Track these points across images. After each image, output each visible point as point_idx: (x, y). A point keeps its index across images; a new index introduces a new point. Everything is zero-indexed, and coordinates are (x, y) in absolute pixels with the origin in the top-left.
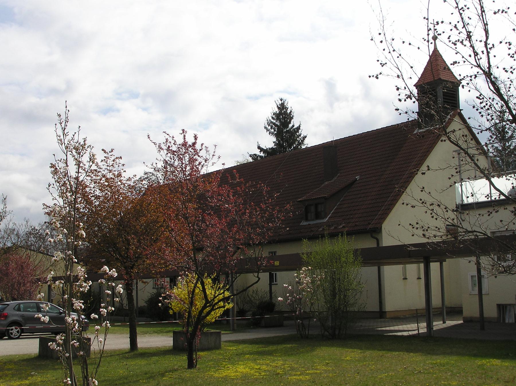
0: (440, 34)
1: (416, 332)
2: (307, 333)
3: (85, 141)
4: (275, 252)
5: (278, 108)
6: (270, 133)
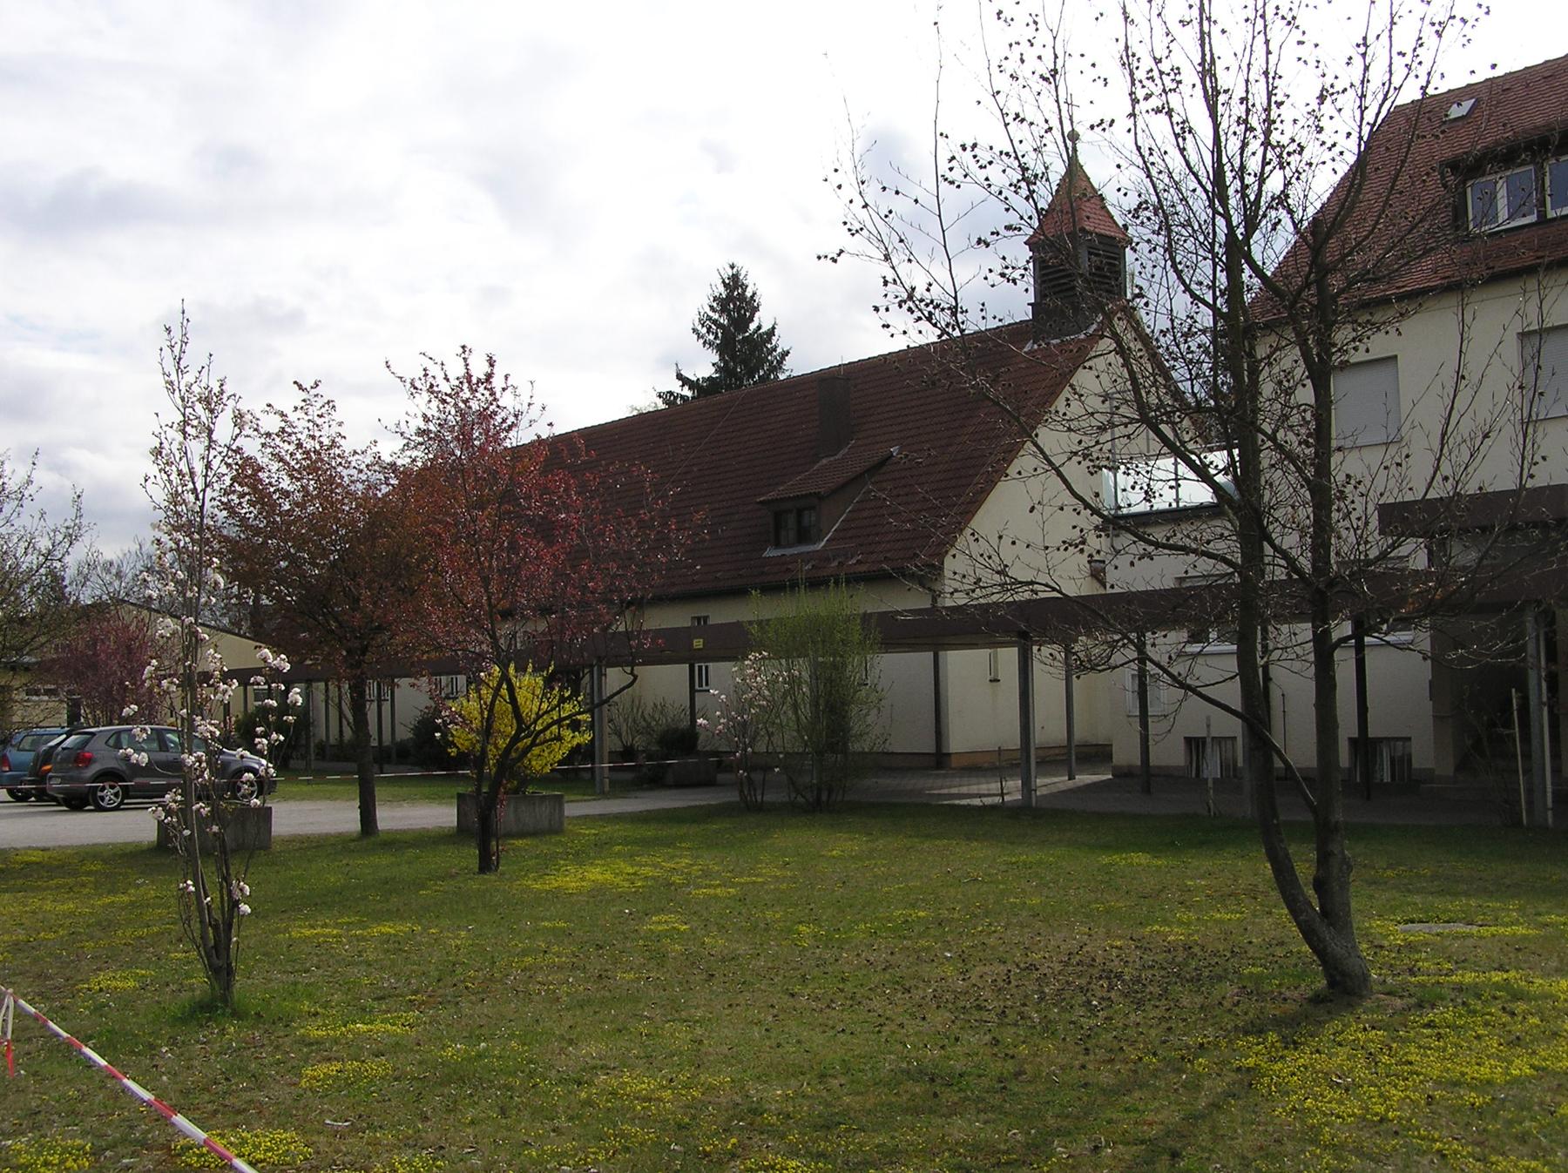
0: (985, 167)
1: (998, 800)
2: (759, 798)
3: (222, 385)
4: (706, 618)
5: (725, 285)
6: (705, 343)
